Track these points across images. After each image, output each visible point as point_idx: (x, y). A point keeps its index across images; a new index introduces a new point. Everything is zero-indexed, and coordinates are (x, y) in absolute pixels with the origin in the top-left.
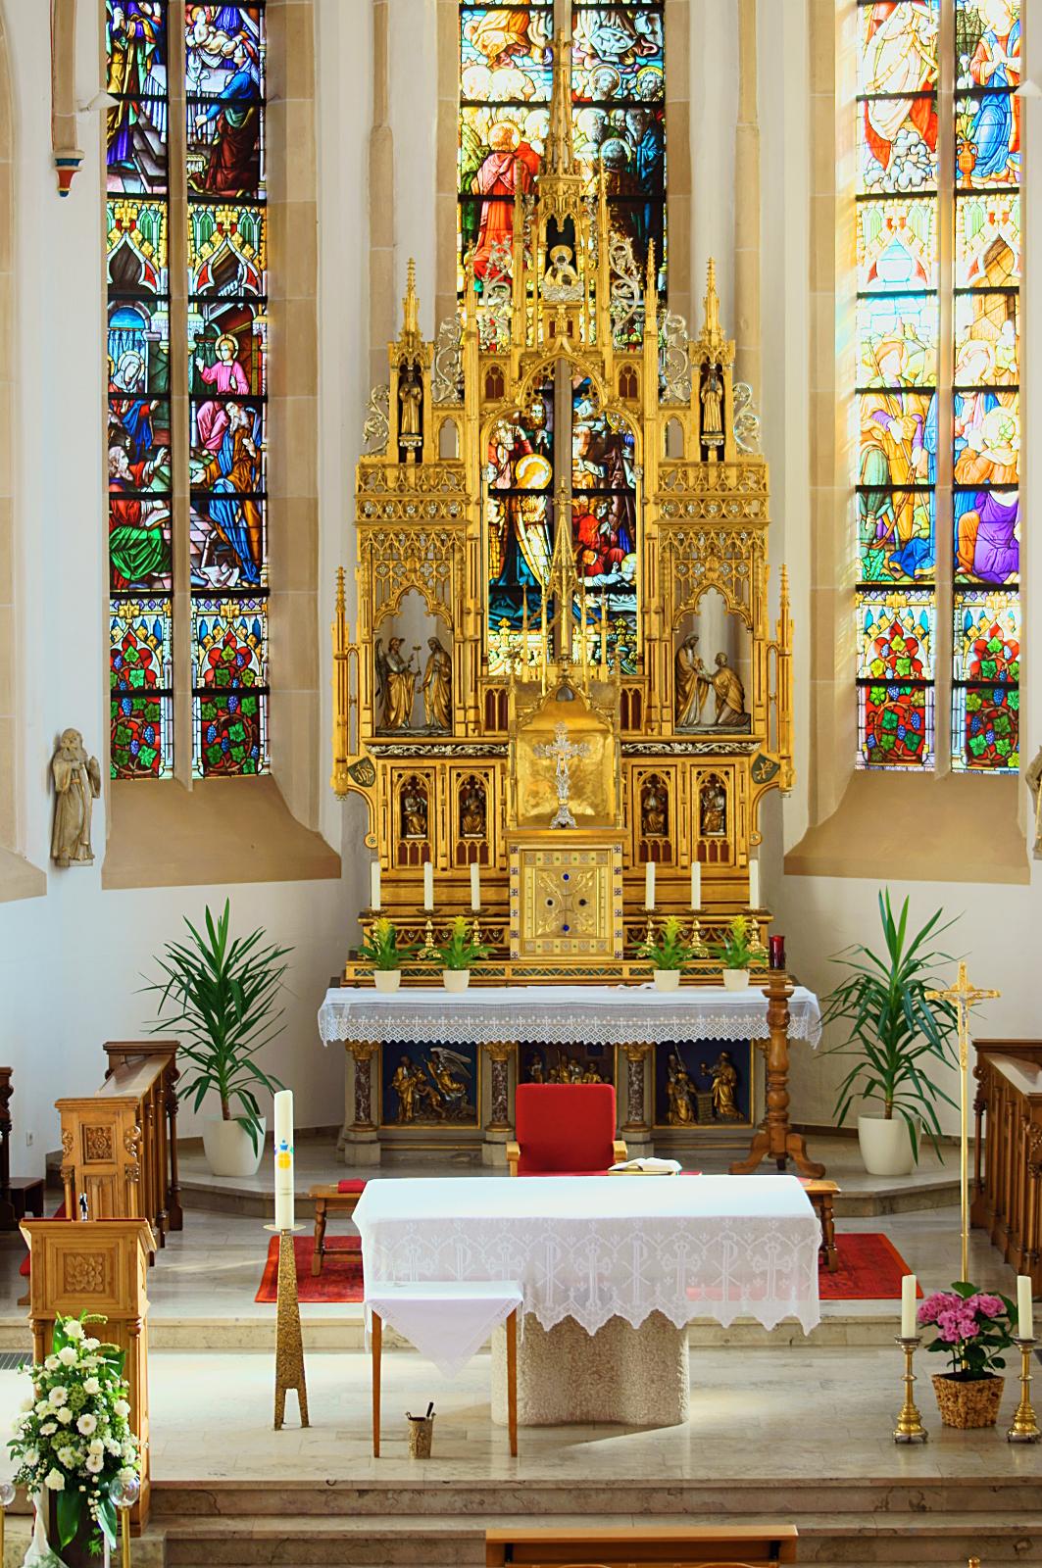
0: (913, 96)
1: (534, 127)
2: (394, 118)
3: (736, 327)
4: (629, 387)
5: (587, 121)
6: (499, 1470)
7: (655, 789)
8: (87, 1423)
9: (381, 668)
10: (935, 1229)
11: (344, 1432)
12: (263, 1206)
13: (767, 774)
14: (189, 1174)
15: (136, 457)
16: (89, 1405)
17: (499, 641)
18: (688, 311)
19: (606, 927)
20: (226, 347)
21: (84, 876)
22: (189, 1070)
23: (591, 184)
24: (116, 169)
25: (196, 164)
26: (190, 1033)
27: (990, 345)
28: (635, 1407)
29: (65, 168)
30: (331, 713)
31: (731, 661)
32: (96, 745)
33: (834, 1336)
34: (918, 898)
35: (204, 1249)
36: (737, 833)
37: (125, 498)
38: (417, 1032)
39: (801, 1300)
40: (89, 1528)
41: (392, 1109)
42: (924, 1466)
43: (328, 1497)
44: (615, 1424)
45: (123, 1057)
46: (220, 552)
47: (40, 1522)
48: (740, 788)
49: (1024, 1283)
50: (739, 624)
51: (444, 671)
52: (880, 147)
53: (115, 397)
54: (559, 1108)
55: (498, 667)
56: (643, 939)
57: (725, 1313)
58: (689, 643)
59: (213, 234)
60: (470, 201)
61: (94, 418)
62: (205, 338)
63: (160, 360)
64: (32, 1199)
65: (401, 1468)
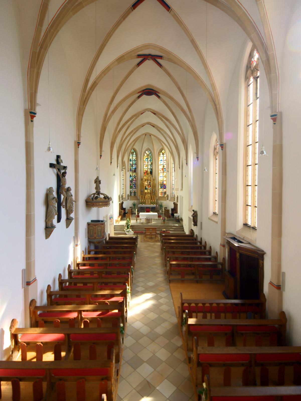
0: (249, 125)
1: (147, 170)
2: (141, 169)
3: (155, 178)
4: (151, 180)
5: (149, 169)
6: (145, 225)
7: (152, 197)
8: (128, 223)
9: (141, 192)
10: (181, 245)
11: (139, 223)
12: (136, 214)
13: (156, 196)
14: (133, 212)
15: (131, 183)
16: (128, 222)
17: (145, 191)
18: (153, 177)
19: (150, 202)
20: (135, 179)
21: (129, 200)
22: (133, 208)
23: (149, 172)
24: (130, 171)
25: (133, 171)
26: (133, 206)
27: (165, 179)
28: (150, 222)
29: (128, 171)
30: (139, 193)
31: (155, 192)
32: (129, 195)
33: (158, 219)
34: (162, 201)
35: (134, 215)
36: (155, 198)
37: (131, 184)
38: (142, 207)
39: (157, 218)
40: (128, 227)
41: (141, 210)
42: (161, 225)
43: (138, 226)
44: (149, 223)
45: (130, 207)
46: (134, 187)
47: (126, 227)
48: (155, 197)
49: (166, 217)
50: (155, 190)
51: (143, 191)
52: (161, 171)
53: (130, 180)
54: (148, 210)
55: (145, 192)
56: (151, 203)
57: (154, 218)
58: (153, 191)
59: (134, 174)
60: (144, 173)
61: (129, 181)
62: (134, 178)
63: (132, 179)
64: (127, 213)
65: (141, 225)
